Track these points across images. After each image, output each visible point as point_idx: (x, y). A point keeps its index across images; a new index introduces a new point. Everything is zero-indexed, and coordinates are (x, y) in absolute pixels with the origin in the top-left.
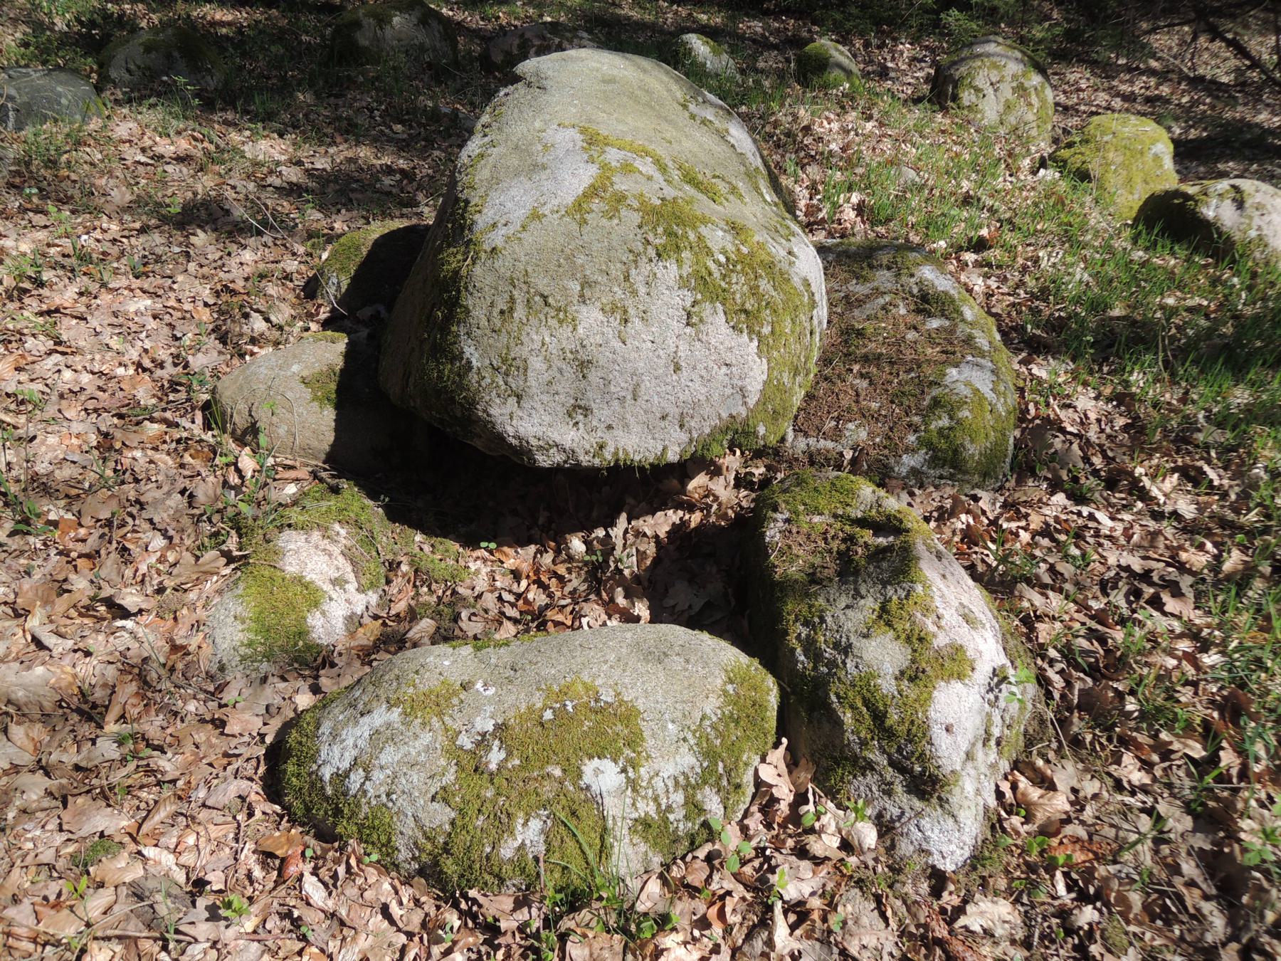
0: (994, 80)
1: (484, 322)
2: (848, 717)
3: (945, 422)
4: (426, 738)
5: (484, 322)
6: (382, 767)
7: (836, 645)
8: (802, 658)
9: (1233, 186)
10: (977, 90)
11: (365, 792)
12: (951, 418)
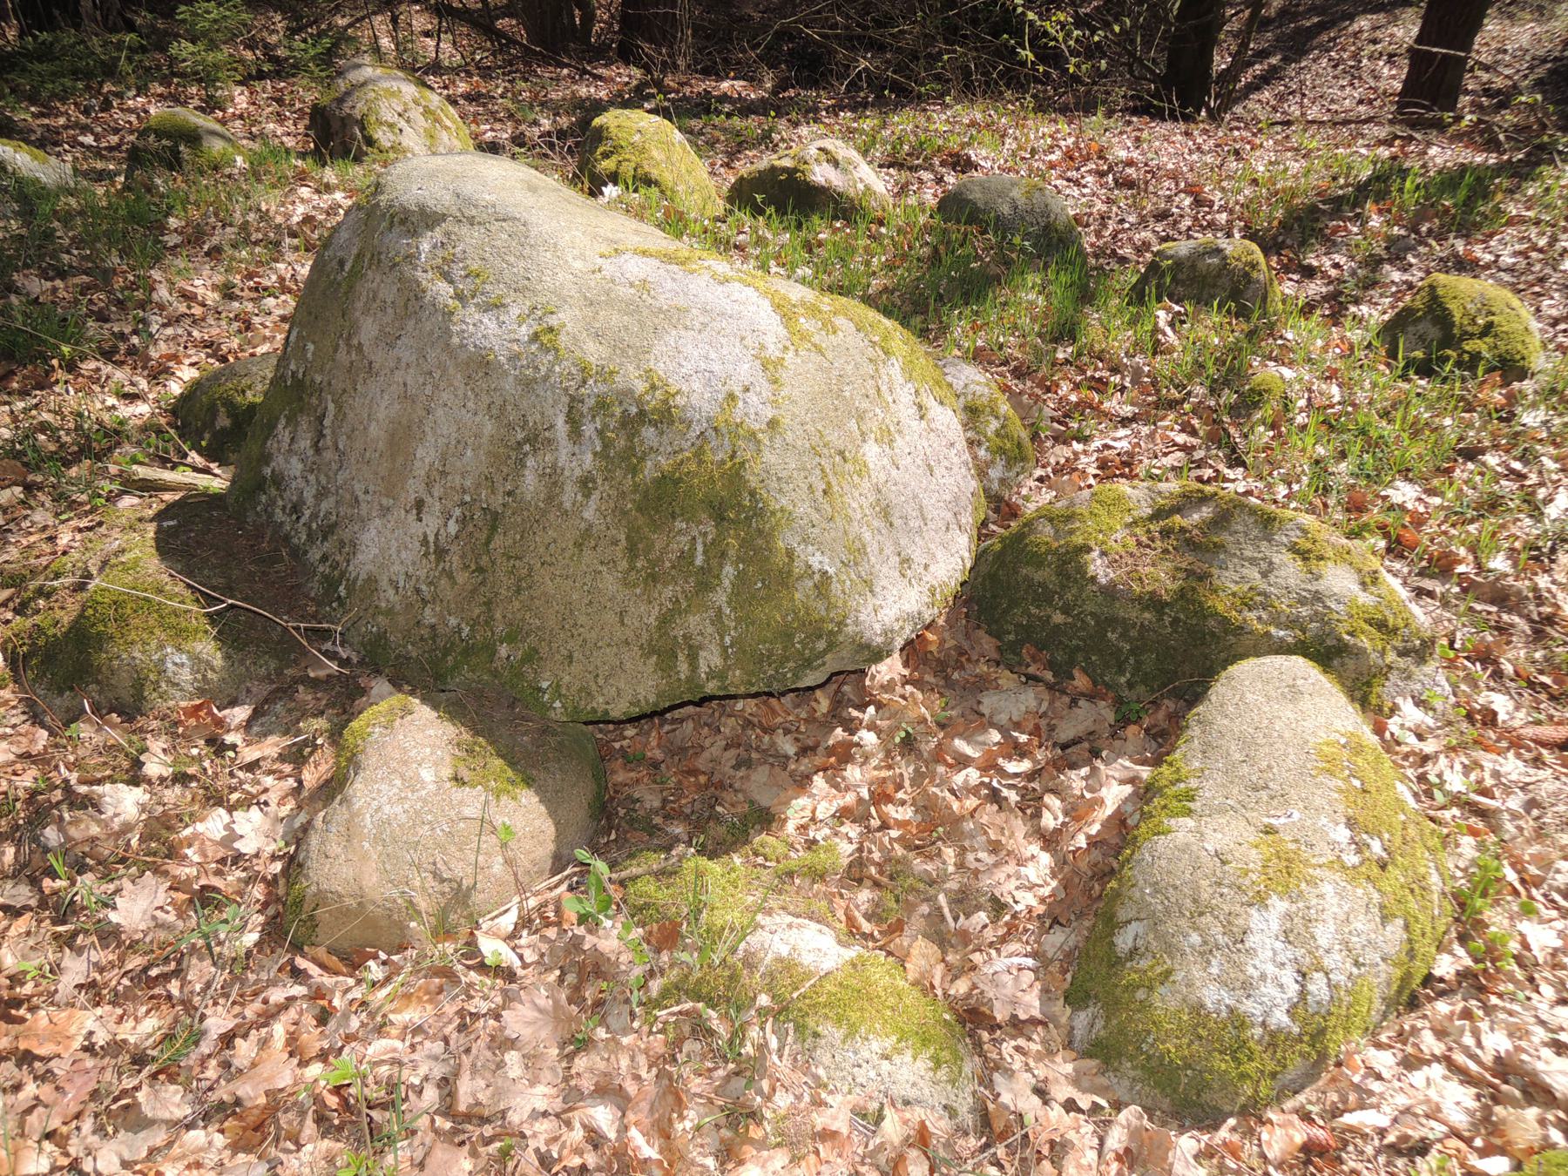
0: (400, 109)
1: (815, 516)
2: (1364, 642)
3: (994, 425)
4: (1327, 889)
5: (815, 516)
6: (1327, 952)
7: (1302, 601)
8: (1282, 633)
9: (820, 149)
10: (391, 126)
11: (1337, 987)
12: (997, 418)
